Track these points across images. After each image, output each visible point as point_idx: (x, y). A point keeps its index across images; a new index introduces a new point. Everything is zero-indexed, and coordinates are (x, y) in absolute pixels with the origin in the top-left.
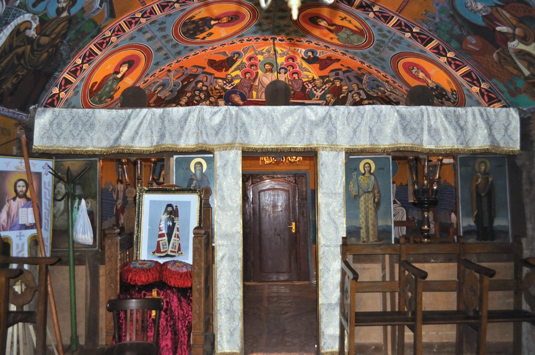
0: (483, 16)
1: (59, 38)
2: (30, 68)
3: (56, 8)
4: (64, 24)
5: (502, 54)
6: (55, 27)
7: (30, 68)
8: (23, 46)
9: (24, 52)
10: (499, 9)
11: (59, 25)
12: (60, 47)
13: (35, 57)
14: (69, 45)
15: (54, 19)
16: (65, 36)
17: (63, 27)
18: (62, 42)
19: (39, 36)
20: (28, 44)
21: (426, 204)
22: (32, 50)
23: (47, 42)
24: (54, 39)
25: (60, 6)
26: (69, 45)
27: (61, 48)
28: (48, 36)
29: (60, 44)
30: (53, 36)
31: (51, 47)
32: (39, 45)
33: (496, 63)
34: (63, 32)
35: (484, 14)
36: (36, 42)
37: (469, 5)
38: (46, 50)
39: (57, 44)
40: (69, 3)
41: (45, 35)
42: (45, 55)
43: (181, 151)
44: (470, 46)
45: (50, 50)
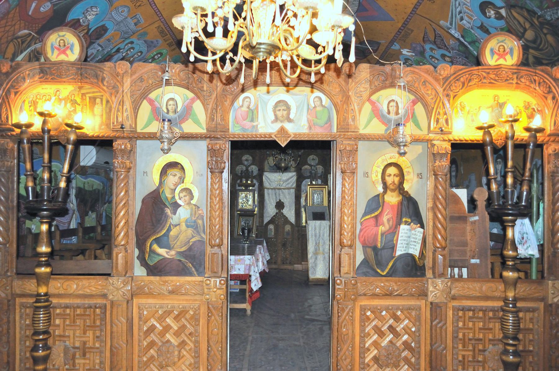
0: (79, 20)
1: (532, 19)
2: (556, 58)
3: (495, 20)
4: (515, 14)
5: (29, 39)
6: (516, 23)
7: (556, 58)
8: (528, 54)
9: (535, 57)
10: (86, 31)
11: (515, 18)
12: (546, 19)
13: (547, 48)
14: (548, 7)
15: (507, 22)
16: (532, 13)
17: (518, 13)
18: (539, 17)
19: (523, 39)
20: (528, 51)
21: (45, 210)
22: (537, 49)
23: (533, 33)
24: (532, 25)
25: (493, 16)
26: (548, 7)
27: (549, 18)
28: (525, 30)
29: (540, 19)
30: (527, 25)
31: (542, 30)
32: (534, 41)
33: (14, 35)
34: (526, 14)
35: (81, 20)
36: (528, 44)
37: (94, 9)
38: (542, 36)
39: (540, 23)
40: (490, 8)
41: (523, 34)
42: (550, 38)
43: (417, 137)
44: (34, 5)
45: (545, 31)
